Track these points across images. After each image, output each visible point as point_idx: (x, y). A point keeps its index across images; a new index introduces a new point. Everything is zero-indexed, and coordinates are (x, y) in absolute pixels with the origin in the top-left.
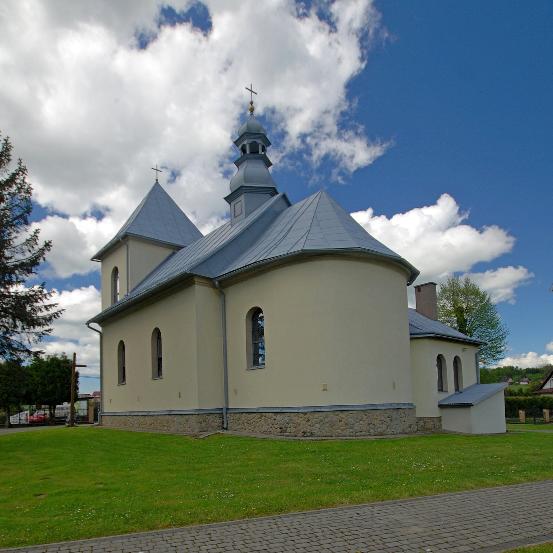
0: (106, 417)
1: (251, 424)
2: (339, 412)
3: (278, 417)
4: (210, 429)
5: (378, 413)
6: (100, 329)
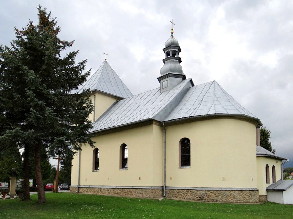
1: (181, 195)
3: (198, 192)
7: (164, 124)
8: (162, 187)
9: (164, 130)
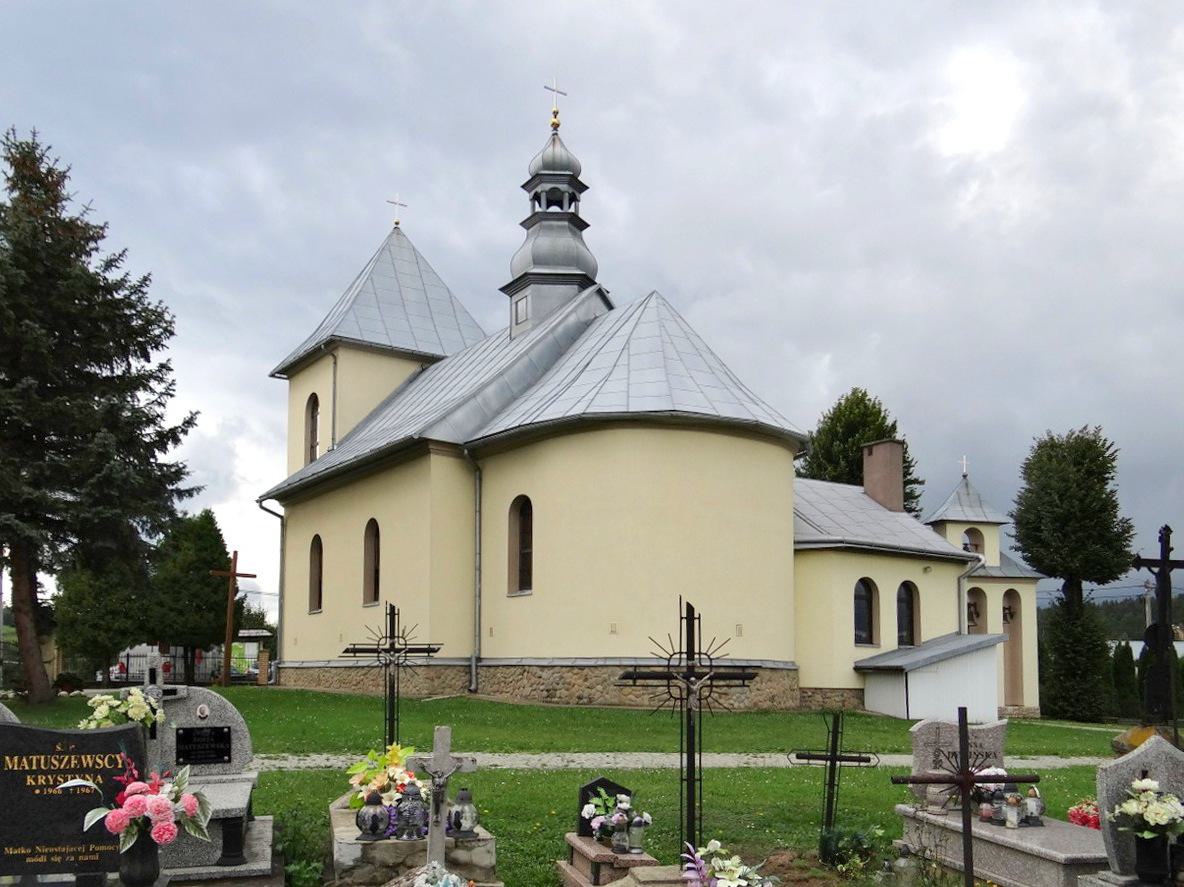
0: (286, 670)
3: (545, 674)
4: (448, 690)
6: (281, 510)
7: (466, 452)
8: (469, 659)
9: (476, 471)
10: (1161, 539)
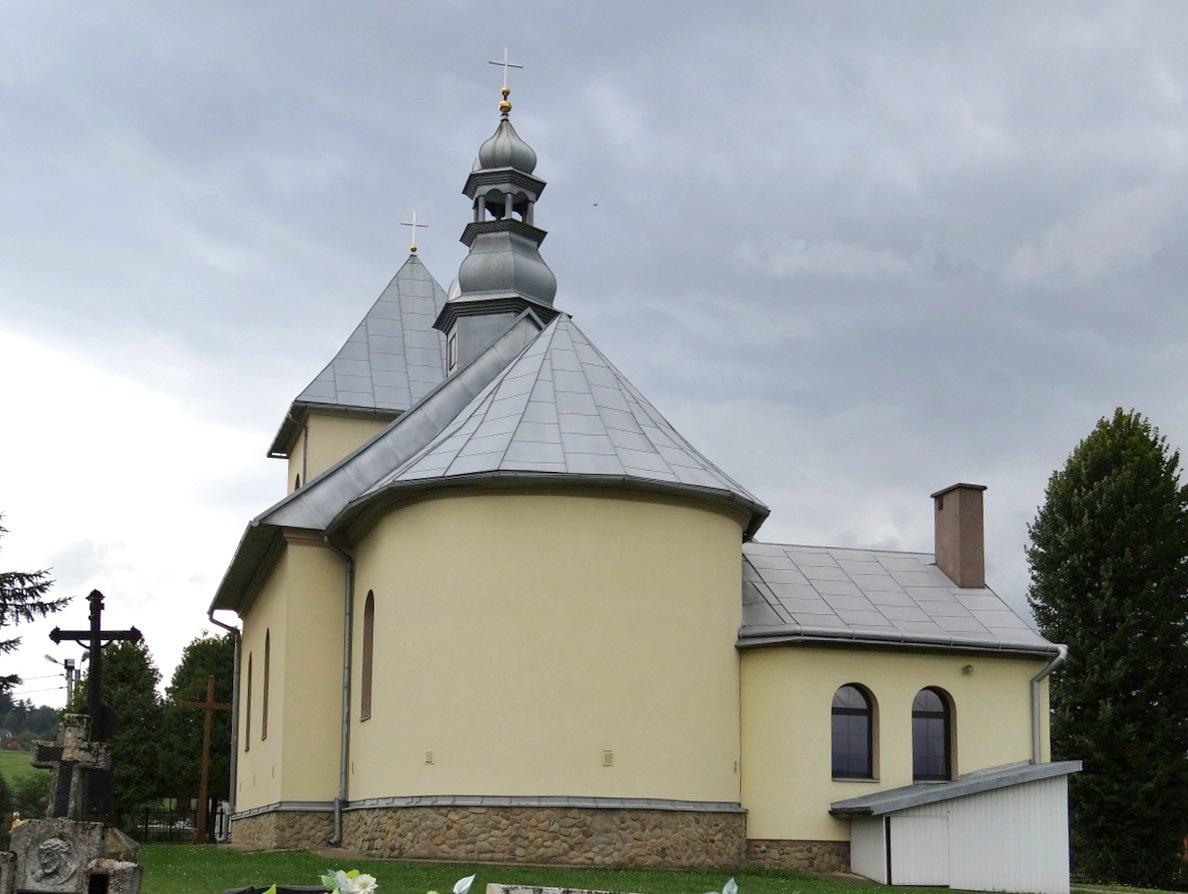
2: (449, 809)
5: (541, 815)
8: (331, 803)
10: (102, 606)
